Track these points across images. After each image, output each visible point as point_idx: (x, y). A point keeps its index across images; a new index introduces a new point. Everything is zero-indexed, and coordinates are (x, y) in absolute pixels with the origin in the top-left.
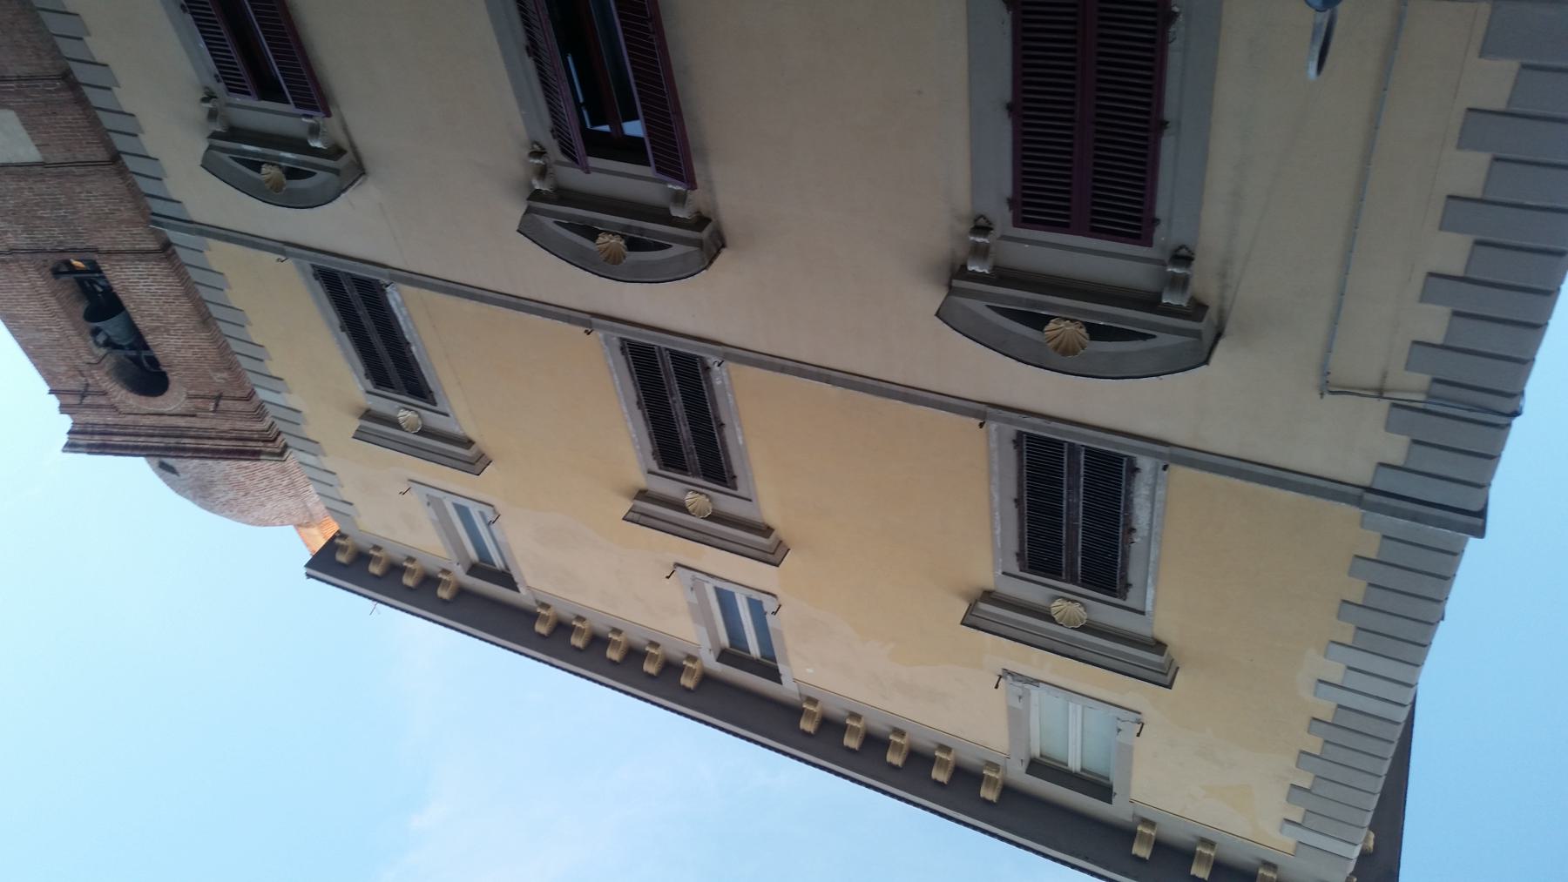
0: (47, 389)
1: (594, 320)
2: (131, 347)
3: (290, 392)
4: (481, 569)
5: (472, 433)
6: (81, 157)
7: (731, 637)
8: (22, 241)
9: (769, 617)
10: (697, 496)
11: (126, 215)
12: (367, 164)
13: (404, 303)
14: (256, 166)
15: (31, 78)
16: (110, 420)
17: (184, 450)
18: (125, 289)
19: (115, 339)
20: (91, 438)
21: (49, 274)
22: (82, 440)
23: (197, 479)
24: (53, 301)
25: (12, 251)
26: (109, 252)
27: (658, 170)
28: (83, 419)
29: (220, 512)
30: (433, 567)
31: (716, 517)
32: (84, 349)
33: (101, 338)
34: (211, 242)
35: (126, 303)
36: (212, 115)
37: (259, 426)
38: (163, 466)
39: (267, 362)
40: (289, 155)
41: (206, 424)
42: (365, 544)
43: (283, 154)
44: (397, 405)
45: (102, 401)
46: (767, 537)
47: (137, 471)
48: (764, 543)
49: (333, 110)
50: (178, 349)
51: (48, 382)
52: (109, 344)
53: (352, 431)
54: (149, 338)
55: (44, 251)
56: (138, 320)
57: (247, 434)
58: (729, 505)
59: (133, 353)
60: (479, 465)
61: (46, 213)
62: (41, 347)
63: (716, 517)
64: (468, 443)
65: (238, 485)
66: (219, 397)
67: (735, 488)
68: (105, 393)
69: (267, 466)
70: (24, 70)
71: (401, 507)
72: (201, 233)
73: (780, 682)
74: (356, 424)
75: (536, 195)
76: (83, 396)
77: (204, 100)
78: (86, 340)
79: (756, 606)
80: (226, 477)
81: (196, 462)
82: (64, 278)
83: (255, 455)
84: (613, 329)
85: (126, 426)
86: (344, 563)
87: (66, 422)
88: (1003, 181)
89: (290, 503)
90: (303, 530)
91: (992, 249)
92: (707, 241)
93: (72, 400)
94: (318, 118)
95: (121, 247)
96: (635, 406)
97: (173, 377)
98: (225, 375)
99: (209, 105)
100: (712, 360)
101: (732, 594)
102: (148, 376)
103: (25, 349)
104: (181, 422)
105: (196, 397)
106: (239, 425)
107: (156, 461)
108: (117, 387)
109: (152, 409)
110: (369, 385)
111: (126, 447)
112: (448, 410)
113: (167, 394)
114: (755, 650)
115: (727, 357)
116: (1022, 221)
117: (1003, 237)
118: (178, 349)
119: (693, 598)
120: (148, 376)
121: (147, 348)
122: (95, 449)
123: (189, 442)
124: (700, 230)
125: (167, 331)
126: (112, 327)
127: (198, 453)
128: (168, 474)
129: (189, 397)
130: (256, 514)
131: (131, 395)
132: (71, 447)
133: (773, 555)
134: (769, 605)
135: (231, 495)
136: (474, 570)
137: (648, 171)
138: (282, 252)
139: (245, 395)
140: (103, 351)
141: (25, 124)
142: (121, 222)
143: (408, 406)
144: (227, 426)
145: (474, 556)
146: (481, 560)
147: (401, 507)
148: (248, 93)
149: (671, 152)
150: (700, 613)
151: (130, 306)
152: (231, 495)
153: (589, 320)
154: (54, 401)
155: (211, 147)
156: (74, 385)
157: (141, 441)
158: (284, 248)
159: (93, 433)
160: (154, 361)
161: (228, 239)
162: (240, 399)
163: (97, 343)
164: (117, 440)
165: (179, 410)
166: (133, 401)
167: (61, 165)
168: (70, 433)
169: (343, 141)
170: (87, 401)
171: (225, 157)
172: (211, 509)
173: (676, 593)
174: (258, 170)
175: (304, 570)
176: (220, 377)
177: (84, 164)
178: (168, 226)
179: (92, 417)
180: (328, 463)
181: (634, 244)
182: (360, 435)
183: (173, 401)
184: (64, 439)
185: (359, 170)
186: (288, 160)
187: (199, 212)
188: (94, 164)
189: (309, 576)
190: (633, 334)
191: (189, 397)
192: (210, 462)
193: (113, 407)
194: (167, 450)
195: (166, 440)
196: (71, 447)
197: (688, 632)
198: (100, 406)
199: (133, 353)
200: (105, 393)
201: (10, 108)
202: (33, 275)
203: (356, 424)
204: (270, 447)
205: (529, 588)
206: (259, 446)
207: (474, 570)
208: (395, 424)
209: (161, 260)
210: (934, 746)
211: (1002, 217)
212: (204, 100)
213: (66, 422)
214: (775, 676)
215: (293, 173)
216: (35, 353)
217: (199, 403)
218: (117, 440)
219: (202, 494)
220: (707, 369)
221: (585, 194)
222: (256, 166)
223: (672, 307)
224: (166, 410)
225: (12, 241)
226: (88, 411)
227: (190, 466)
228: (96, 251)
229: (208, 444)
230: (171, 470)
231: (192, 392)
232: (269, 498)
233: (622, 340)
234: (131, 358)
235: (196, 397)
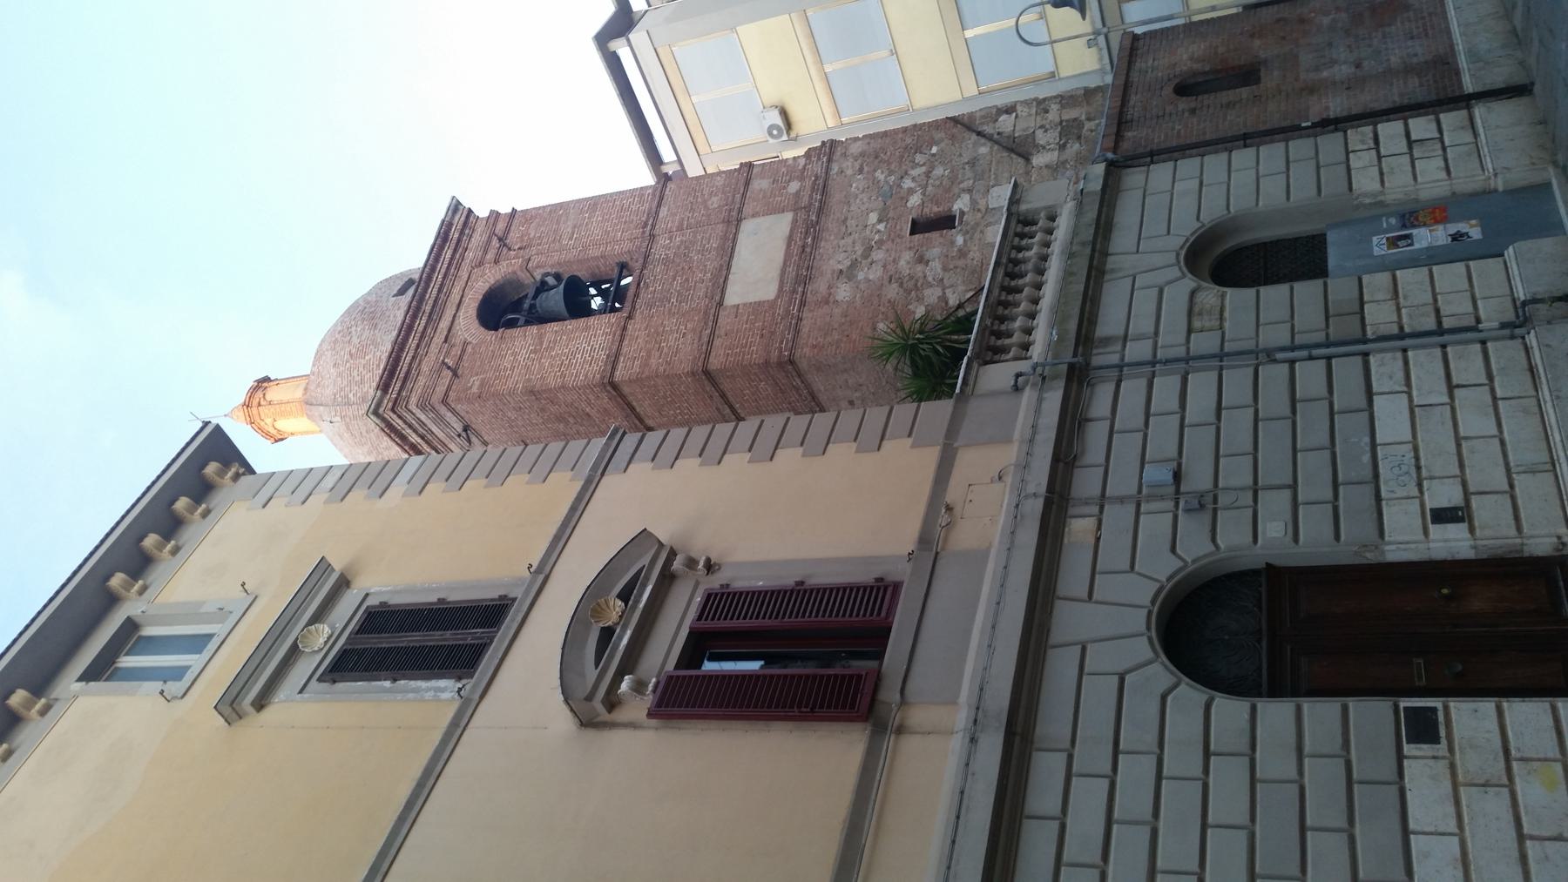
0: (519, 209)
1: (541, 577)
2: (532, 306)
3: (405, 495)
4: (129, 638)
5: (272, 713)
6: (717, 342)
7: (150, 638)
8: (659, 251)
9: (159, 685)
10: (322, 639)
11: (653, 361)
12: (591, 734)
13: (437, 700)
14: (625, 596)
15: (797, 331)
16: (470, 255)
17: (414, 317)
18: (587, 328)
19: (544, 295)
20: (457, 228)
21: (624, 259)
22: (459, 220)
23: (383, 314)
24: (597, 253)
25: (652, 237)
26: (625, 328)
27: (670, 678)
28: (480, 229)
29: (342, 321)
30: (156, 575)
31: (294, 651)
32: (545, 260)
33: (551, 281)
34: (578, 485)
35: (574, 322)
36: (691, 563)
37: (414, 400)
38: (411, 282)
39: (444, 485)
40: (625, 641)
41: (434, 348)
42: (216, 499)
43: (629, 633)
44: (339, 626)
45: (490, 256)
46: (253, 704)
47: (414, 258)
48: (248, 696)
49: (654, 722)
50: (515, 354)
51: (525, 212)
52: (543, 287)
53: (330, 559)
54: (534, 329)
55: (644, 267)
56: (554, 326)
57: (409, 385)
58: (303, 669)
59: (526, 306)
60: (227, 711)
61: (677, 285)
62: (558, 222)
63: (294, 651)
64: (260, 704)
65: (362, 351)
66: (455, 374)
67: (320, 680)
68: (496, 262)
69: (370, 388)
70: (805, 330)
71: (229, 575)
72: (588, 482)
73: (80, 679)
74: (338, 566)
75: (673, 554)
76: (500, 240)
77: (708, 560)
78: (552, 266)
79: (177, 673)
80: (375, 343)
81: (400, 318)
82: (616, 271)
83: (384, 386)
84: (527, 592)
85: (458, 268)
86: (208, 466)
87: (482, 212)
88: (740, 584)
89: (328, 392)
90: (303, 383)
91: (691, 573)
92: (593, 710)
93: (501, 226)
94: (649, 699)
95: (626, 342)
96: (442, 596)
97: (490, 335)
98: (475, 389)
99: (701, 564)
100: (469, 684)
101: (200, 652)
102: (499, 311)
103: (561, 205)
104: (444, 324)
105: (464, 351)
106: (422, 381)
107: (416, 277)
108: (498, 277)
109: (466, 300)
110: (373, 601)
111: (437, 260)
112: (305, 695)
113: (476, 323)
114: (127, 661)
115: (466, 702)
116: (709, 596)
117: (697, 584)
118: (515, 354)
119: (210, 608)
120: (499, 311)
121: (528, 323)
122: (443, 237)
123: (421, 324)
124: (603, 702)
125: (534, 352)
126: (555, 299)
127: (406, 330)
128: (400, 284)
129: (466, 344)
130: (329, 354)
131: (487, 286)
132: (456, 207)
133: (231, 706)
134: (174, 687)
135: (355, 340)
136: (131, 626)
137: (670, 666)
138: (539, 570)
139: (450, 400)
140: (538, 278)
141: (759, 303)
142: (649, 355)
143: (331, 640)
144: (425, 368)
145: (148, 631)
146: (117, 669)
147: (229, 575)
148: (700, 618)
149: (686, 699)
150: (192, 612)
151: (571, 325)
152: (355, 340)
153: (543, 573)
154: (505, 209)
155: (661, 545)
156: (513, 237)
157: (438, 277)
158: (543, 573)
159: (462, 233)
160: (512, 324)
161: (579, 498)
162: (446, 395)
163: (547, 274)
164: (447, 253)
165: (456, 327)
166: (480, 286)
167: (716, 321)
168: (470, 211)
169: (621, 715)
170: (495, 243)
171: (646, 560)
172: (348, 312)
173: (225, 591)
174: (619, 596)
175: (214, 422)
176: (475, 383)
177: (710, 343)
178: (607, 444)
179: (478, 238)
180: (317, 500)
181: (607, 634)
182: (323, 566)
183: (467, 325)
184: (467, 203)
185: (587, 722)
186: (620, 638)
187: (611, 485)
188: (708, 353)
189: (206, 424)
190: (509, 627)
191: (466, 344)
192: (395, 333)
193: (481, 264)
194: (422, 294)
195: (431, 302)
196: (456, 207)
197: (187, 583)
198: (486, 252)
199: (526, 306)
200: (496, 262)
201: (778, 297)
202: (626, 246)
203: (338, 566)
204: (387, 403)
205: (76, 697)
206: (393, 393)
207: (131, 626)
208: (317, 618)
209: (603, 378)
210: (14, 745)
211: (715, 582)
212: (708, 560)
213: (482, 212)
214: (90, 675)
215: (607, 634)
216: (554, 213)
217: (456, 351)
218: (447, 253)
219: (365, 312)
220: (459, 679)
221: (662, 602)
222: (625, 596)
223: (533, 660)
224: (461, 314)
225: (662, 241)
226: (484, 238)
227: (397, 311)
228: (630, 317)
229: (412, 342)
230: (402, 292)
231: (469, 349)
232: (340, 375)
233: (514, 600)
234: (520, 301)
235: (464, 351)
